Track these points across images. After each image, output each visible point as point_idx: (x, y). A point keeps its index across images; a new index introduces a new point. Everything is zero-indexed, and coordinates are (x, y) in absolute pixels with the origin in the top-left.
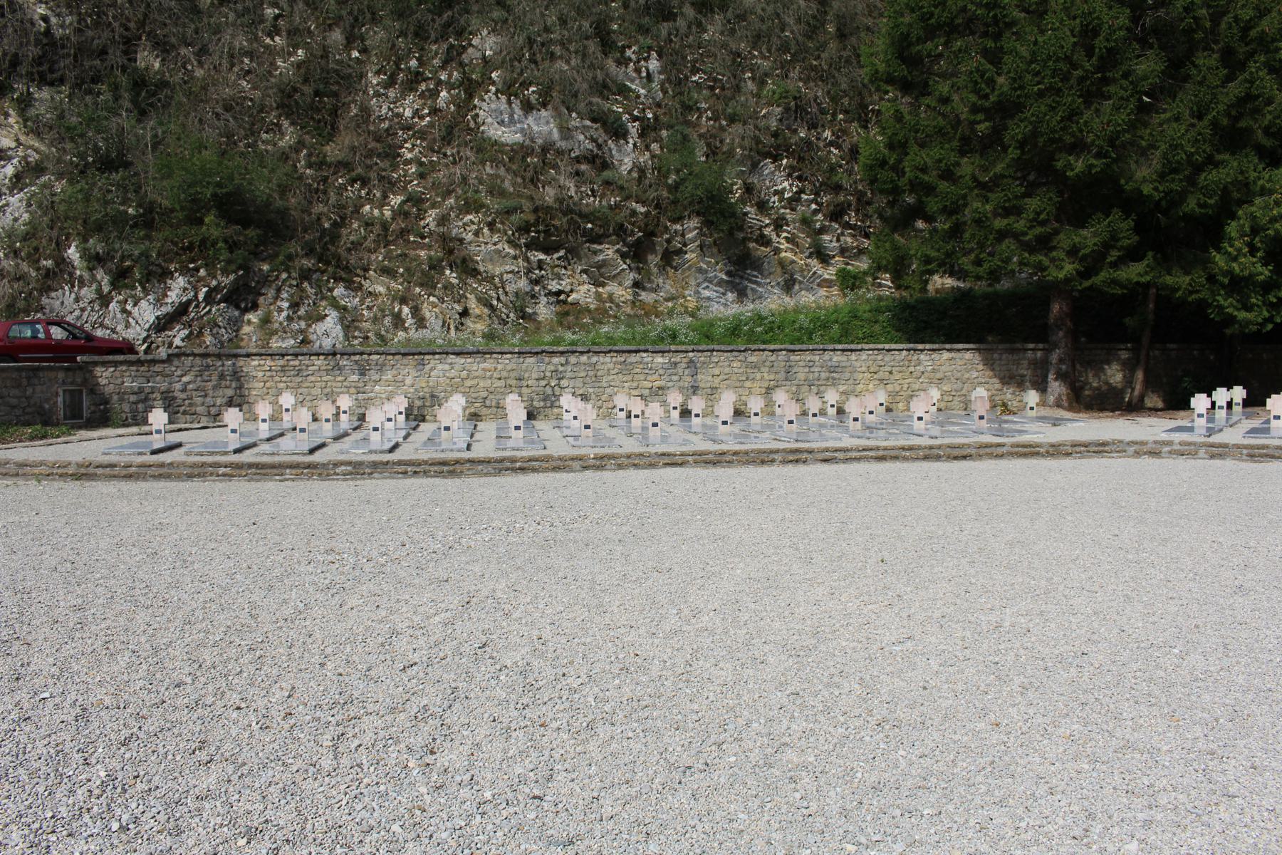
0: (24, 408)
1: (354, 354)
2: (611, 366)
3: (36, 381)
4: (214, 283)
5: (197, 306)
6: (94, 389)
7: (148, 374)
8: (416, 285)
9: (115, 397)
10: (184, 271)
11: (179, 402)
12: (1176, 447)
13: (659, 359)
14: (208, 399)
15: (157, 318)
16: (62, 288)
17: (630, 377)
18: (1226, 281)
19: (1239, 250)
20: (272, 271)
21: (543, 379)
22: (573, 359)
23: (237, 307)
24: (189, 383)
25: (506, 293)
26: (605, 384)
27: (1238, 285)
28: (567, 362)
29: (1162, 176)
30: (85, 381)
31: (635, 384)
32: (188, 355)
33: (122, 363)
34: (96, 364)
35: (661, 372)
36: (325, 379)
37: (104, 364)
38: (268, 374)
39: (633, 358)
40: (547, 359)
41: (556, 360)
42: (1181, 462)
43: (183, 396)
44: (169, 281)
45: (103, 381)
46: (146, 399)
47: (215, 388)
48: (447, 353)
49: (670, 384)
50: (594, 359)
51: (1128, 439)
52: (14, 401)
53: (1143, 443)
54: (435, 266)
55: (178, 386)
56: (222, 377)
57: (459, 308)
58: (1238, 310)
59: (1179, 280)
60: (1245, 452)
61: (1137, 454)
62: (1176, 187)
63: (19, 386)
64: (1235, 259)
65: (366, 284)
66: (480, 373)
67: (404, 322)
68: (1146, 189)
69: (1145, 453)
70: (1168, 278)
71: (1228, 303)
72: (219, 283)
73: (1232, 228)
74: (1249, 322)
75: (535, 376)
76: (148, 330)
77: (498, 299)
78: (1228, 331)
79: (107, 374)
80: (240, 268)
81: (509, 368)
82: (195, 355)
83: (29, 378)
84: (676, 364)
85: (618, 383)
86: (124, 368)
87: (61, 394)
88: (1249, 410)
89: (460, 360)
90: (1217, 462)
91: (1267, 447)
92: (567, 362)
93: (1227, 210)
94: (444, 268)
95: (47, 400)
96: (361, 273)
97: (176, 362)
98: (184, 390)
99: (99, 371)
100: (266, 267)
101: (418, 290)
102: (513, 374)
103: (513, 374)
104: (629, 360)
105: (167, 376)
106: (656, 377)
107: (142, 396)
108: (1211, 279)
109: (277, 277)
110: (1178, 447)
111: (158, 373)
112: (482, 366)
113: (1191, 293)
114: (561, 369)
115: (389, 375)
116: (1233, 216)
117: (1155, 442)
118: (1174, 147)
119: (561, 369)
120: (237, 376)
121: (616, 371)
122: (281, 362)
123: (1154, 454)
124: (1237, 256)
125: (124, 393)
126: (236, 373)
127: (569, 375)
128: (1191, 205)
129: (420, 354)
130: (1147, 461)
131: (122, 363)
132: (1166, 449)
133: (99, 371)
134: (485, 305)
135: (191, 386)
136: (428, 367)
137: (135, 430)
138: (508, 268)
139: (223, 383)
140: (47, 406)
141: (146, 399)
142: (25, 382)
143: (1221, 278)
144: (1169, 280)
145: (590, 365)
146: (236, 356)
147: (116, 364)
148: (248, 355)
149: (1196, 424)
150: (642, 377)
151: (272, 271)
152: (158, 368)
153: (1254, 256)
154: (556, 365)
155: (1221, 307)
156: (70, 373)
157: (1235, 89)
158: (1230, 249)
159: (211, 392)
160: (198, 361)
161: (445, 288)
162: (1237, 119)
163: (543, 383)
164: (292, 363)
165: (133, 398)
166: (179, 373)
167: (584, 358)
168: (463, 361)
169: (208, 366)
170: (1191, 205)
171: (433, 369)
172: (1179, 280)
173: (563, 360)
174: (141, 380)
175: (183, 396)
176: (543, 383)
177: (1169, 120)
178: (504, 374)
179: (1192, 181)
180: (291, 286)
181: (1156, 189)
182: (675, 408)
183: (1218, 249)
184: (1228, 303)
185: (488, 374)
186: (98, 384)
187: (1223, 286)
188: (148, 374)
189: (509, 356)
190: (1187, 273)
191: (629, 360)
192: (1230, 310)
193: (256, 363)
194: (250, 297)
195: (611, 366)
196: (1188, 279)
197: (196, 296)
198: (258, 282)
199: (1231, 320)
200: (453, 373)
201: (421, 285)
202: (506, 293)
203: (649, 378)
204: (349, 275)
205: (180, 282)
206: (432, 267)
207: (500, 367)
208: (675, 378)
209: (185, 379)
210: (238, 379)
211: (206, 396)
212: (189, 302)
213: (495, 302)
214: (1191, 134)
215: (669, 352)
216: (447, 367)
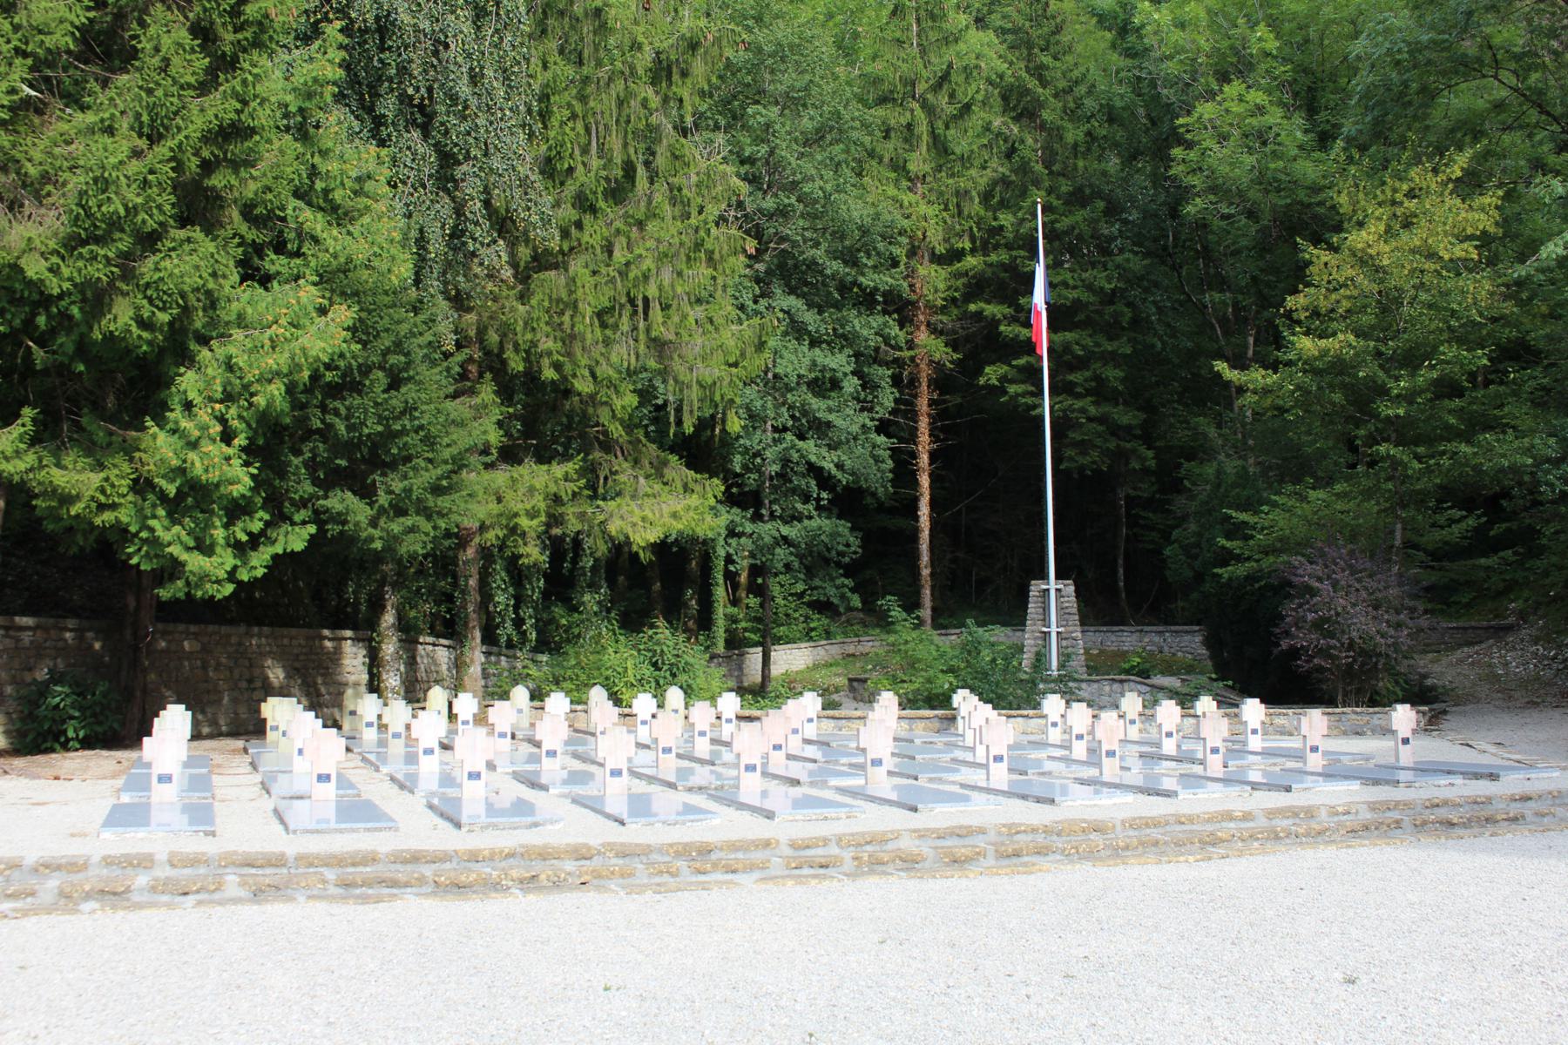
12: (163, 872)
18: (171, 489)
19: (204, 428)
27: (192, 498)
29: (72, 244)
42: (186, 917)
51: (31, 858)
53: (75, 866)
58: (188, 549)
59: (77, 479)
60: (330, 875)
61: (68, 900)
62: (98, 272)
64: (194, 445)
68: (34, 268)
69: (88, 896)
70: (55, 471)
71: (173, 537)
73: (188, 382)
74: (204, 577)
78: (165, 593)
88: (195, 743)
90: (276, 910)
91: (371, 859)
93: (179, 345)
108: (142, 486)
110: (168, 872)
113: (102, 507)
116: (187, 359)
117: (108, 861)
118: (103, 184)
123: (113, 896)
124: (193, 440)
128: (121, 316)
130: (93, 920)
132: (142, 880)
143: (163, 483)
144: (59, 478)
149: (155, 799)
153: (229, 444)
155: (154, 542)
157: (218, 107)
158: (184, 424)
162: (208, 167)
170: (121, 316)
172: (77, 479)
177: (91, 130)
179: (126, 266)
181: (54, 270)
183: (161, 421)
184: (173, 537)
187: (163, 497)
190: (100, 466)
192: (175, 550)
196: (96, 479)
199: (174, 569)
214: (135, 167)
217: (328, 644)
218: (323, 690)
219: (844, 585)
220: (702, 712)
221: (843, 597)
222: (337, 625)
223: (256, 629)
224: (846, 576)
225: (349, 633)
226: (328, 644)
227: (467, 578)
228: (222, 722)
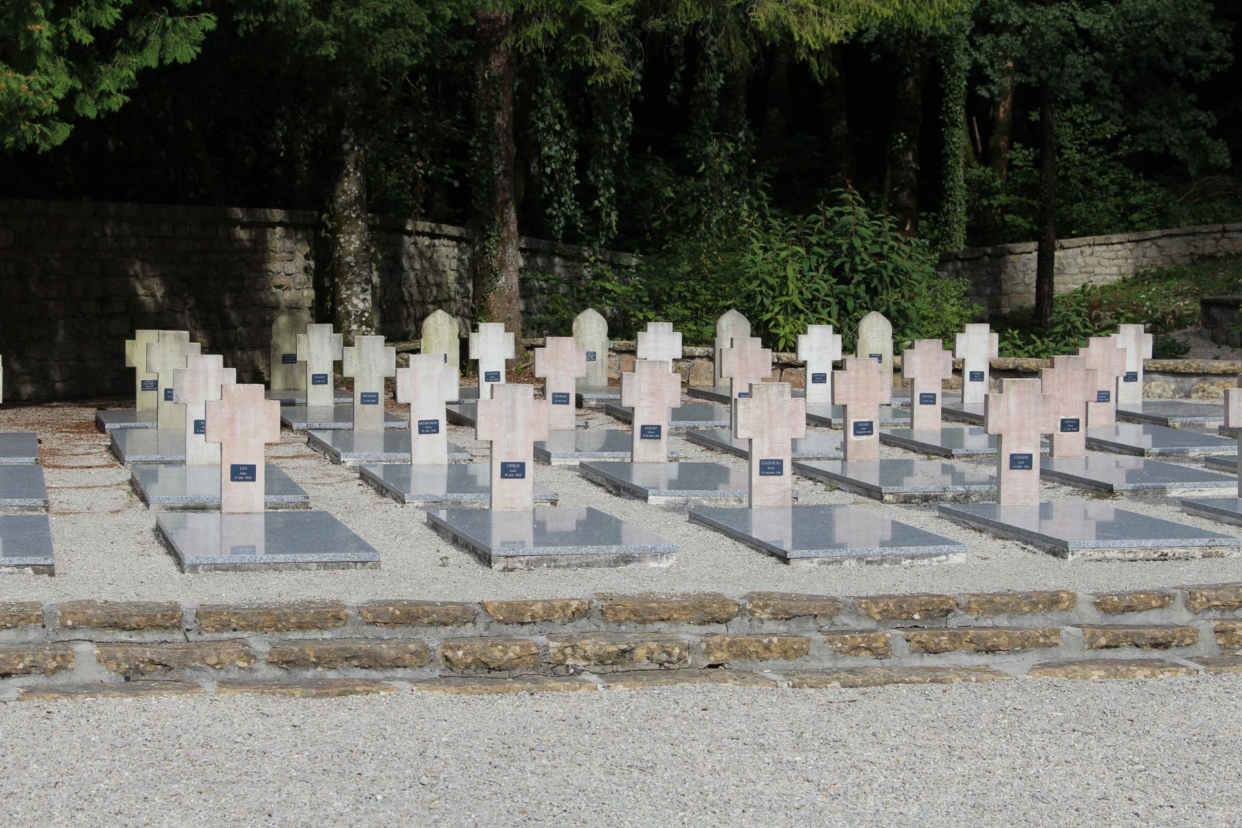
217: (242, 234)
218: (233, 317)
219: (1196, 124)
220: (926, 362)
221: (1195, 144)
222: (256, 201)
223: (111, 208)
224: (1201, 105)
225: (278, 215)
226: (242, 234)
227: (492, 111)
228: (55, 375)
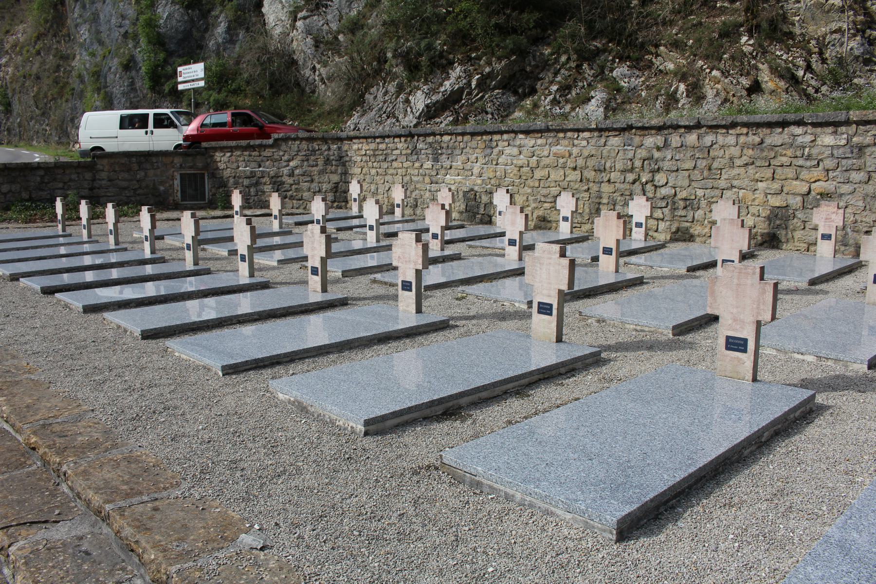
0: (135, 190)
1: (429, 135)
2: (735, 151)
3: (148, 166)
4: (487, 70)
5: (470, 94)
6: (214, 173)
7: (259, 159)
8: (700, 58)
9: (232, 180)
10: (467, 60)
11: (287, 186)
13: (827, 139)
14: (314, 185)
15: (427, 106)
16: (378, 84)
17: (768, 173)
20: (552, 54)
21: (632, 170)
22: (675, 140)
23: (515, 93)
24: (296, 167)
25: (824, 61)
26: (722, 184)
28: (666, 145)
30: (206, 167)
31: (776, 186)
32: (295, 139)
33: (237, 148)
34: (215, 149)
35: (829, 163)
36: (405, 165)
37: (222, 149)
38: (364, 158)
39: (776, 137)
40: (637, 140)
41: (650, 141)
43: (291, 181)
44: (450, 71)
45: (222, 166)
46: (257, 184)
47: (321, 173)
48: (516, 133)
49: (845, 189)
50: (708, 139)
52: (124, 184)
54: (729, 33)
55: (286, 171)
56: (327, 161)
57: (745, 82)
63: (129, 170)
65: (657, 62)
66: (551, 160)
67: (677, 101)
72: (493, 70)
75: (619, 166)
76: (419, 118)
77: (809, 68)
79: (225, 159)
80: (513, 52)
81: (586, 153)
82: (302, 139)
83: (140, 164)
84: (861, 148)
85: (746, 183)
86: (239, 153)
87: (178, 177)
89: (529, 141)
92: (666, 145)
94: (740, 35)
95: (162, 183)
96: (653, 50)
97: (284, 147)
98: (291, 174)
99: (218, 155)
100: (547, 51)
101: (701, 63)
102: (591, 163)
103: (591, 163)
104: (768, 141)
105: (276, 160)
106: (817, 173)
107: (254, 180)
109: (557, 60)
111: (268, 158)
112: (554, 149)
114: (657, 154)
115: (458, 163)
119: (657, 154)
120: (342, 161)
121: (745, 160)
122: (373, 146)
125: (239, 177)
126: (341, 157)
127: (666, 165)
129: (486, 133)
131: (237, 148)
133: (218, 155)
134: (781, 77)
135: (297, 172)
136: (496, 151)
137: (218, 213)
138: (834, 26)
139: (329, 168)
140: (162, 188)
141: (257, 184)
142: (135, 167)
145: (700, 149)
146: (341, 139)
147: (232, 149)
148: (350, 139)
150: (790, 172)
151: (552, 54)
152: (267, 153)
154: (649, 150)
156: (190, 159)
159: (316, 177)
160: (304, 145)
161: (733, 58)
163: (630, 177)
164: (381, 146)
165: (246, 182)
166: (286, 158)
167: (692, 138)
168: (533, 142)
169: (314, 151)
171: (501, 153)
173: (659, 140)
174: (253, 164)
175: (291, 181)
176: (630, 177)
178: (580, 162)
180: (570, 69)
182: (826, 237)
185: (561, 161)
186: (218, 168)
188: (259, 159)
189: (586, 134)
191: (768, 141)
193: (355, 147)
194: (527, 83)
195: (735, 151)
197: (469, 84)
198: (537, 67)
200: (522, 160)
201: (706, 57)
202: (824, 61)
203: (804, 174)
204: (637, 54)
205: (457, 71)
206: (722, 35)
207: (575, 151)
208: (855, 176)
209: (292, 164)
210: (344, 165)
211: (312, 181)
212: (461, 90)
213: (800, 73)
215: (848, 123)
216: (515, 151)
